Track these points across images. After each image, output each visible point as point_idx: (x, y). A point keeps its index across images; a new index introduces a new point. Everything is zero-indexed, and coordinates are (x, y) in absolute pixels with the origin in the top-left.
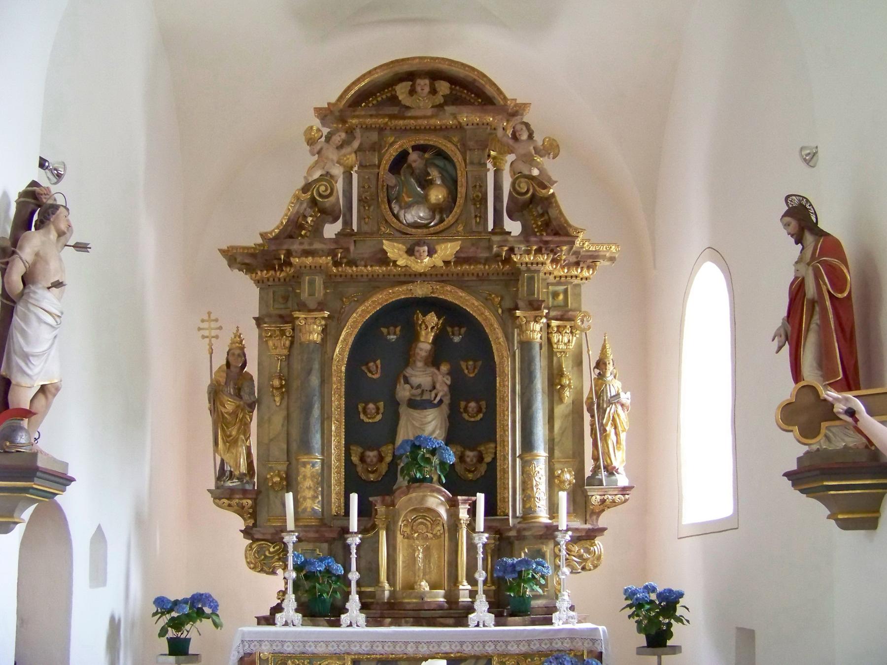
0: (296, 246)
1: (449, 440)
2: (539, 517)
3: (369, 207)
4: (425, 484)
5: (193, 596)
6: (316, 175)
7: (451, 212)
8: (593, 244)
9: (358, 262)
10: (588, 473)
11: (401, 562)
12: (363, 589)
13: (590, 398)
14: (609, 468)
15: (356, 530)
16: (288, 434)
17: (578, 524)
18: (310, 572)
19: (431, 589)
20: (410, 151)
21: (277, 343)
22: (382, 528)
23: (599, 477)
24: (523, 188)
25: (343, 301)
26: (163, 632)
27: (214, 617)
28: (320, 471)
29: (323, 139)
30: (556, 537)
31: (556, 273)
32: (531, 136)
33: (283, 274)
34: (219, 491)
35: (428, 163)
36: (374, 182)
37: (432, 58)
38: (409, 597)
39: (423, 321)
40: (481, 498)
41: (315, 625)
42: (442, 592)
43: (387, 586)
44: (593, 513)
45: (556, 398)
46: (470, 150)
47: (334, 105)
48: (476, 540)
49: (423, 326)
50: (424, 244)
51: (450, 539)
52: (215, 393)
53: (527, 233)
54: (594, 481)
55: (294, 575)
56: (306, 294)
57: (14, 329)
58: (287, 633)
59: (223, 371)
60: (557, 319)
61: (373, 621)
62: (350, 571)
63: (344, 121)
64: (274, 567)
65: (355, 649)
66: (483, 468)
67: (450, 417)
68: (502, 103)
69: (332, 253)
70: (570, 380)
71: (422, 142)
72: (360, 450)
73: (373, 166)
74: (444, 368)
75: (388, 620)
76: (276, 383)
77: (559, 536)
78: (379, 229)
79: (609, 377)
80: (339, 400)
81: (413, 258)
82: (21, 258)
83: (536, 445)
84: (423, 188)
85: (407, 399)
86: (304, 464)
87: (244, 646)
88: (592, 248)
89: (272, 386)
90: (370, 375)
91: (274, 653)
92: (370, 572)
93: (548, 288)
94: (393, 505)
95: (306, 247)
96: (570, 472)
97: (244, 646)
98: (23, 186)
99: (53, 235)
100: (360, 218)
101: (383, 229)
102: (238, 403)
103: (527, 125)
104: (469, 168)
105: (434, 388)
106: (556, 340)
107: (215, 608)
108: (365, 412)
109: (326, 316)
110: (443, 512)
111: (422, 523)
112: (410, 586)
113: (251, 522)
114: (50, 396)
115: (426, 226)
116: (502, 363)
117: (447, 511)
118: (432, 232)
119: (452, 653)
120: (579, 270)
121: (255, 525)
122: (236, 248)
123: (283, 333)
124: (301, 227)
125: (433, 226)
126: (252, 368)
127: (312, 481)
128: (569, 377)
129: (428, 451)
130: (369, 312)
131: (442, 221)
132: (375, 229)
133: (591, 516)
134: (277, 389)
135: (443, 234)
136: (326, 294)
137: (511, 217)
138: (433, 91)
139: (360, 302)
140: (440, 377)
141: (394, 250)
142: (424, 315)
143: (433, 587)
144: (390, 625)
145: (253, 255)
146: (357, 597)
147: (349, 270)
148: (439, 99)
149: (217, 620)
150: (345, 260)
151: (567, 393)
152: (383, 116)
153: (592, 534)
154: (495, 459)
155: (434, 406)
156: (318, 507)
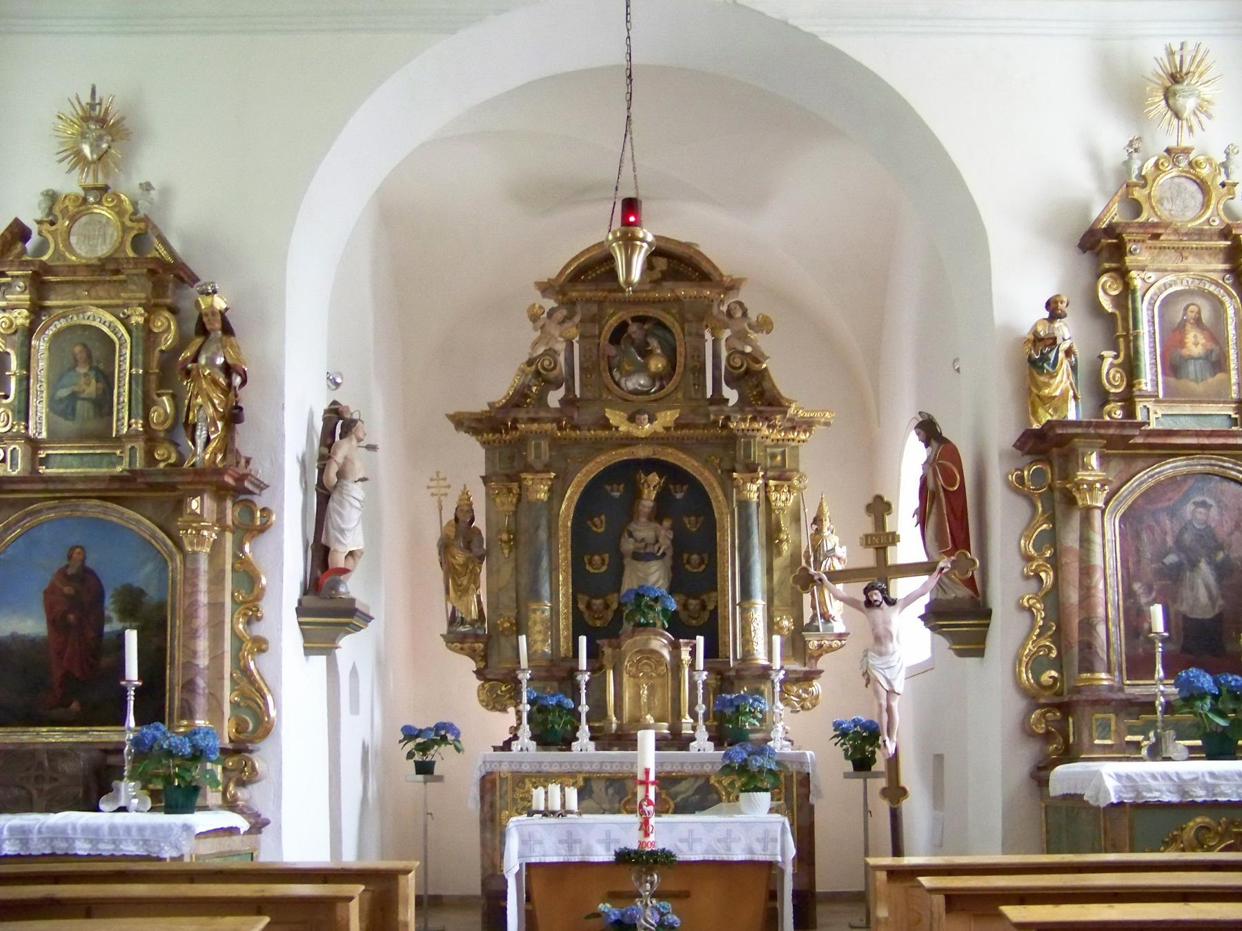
0: (522, 414)
1: (672, 591)
2: (757, 659)
3: (591, 375)
4: (649, 628)
6: (541, 350)
7: (670, 380)
8: (807, 411)
9: (582, 427)
10: (807, 620)
11: (627, 699)
12: (591, 724)
13: (807, 552)
14: (826, 616)
15: (585, 668)
16: (517, 584)
17: (796, 666)
18: (542, 705)
19: (655, 721)
20: (630, 322)
21: (504, 499)
22: (609, 668)
23: (816, 624)
24: (738, 362)
26: (410, 755)
27: (457, 743)
28: (549, 617)
29: (545, 315)
30: (770, 675)
31: (772, 437)
32: (745, 314)
34: (451, 635)
36: (595, 351)
39: (646, 481)
40: (700, 640)
42: (666, 724)
43: (614, 719)
44: (811, 657)
45: (775, 551)
46: (688, 322)
47: (553, 280)
48: (696, 677)
49: (646, 485)
50: (645, 412)
51: (673, 678)
52: (445, 547)
53: (743, 401)
54: (812, 627)
55: (528, 707)
56: (533, 456)
57: (332, 512)
59: (452, 526)
60: (774, 479)
62: (579, 704)
63: (564, 294)
64: (506, 705)
65: (587, 768)
66: (706, 616)
69: (558, 421)
70: (787, 535)
71: (641, 314)
72: (586, 598)
73: (594, 336)
74: (667, 523)
76: (505, 537)
77: (773, 674)
79: (826, 533)
80: (566, 552)
81: (634, 425)
82: (335, 461)
83: (753, 594)
84: (643, 356)
85: (631, 551)
86: (534, 611)
87: (486, 766)
88: (808, 415)
89: (501, 540)
90: (595, 529)
91: (513, 772)
92: (598, 710)
93: (766, 451)
94: (619, 646)
95: (532, 415)
96: (788, 620)
98: (325, 406)
99: (354, 442)
100: (582, 385)
102: (468, 555)
103: (740, 304)
104: (687, 338)
105: (657, 541)
106: (774, 499)
107: (457, 734)
108: (590, 563)
109: (552, 477)
110: (666, 653)
111: (646, 664)
113: (482, 665)
114: (357, 559)
115: (647, 393)
116: (722, 519)
117: (670, 653)
118: (652, 399)
119: (673, 772)
120: (796, 434)
121: (486, 667)
122: (463, 413)
124: (526, 396)
126: (480, 523)
127: (542, 625)
128: (787, 532)
129: (652, 599)
130: (593, 473)
131: (662, 388)
132: (597, 396)
133: (810, 659)
134: (505, 542)
135: (663, 402)
136: (551, 457)
137: (727, 384)
139: (585, 462)
140: (663, 532)
141: (616, 417)
142: (647, 474)
145: (479, 420)
147: (573, 434)
150: (569, 426)
151: (785, 547)
152: (603, 290)
153: (811, 676)
154: (716, 608)
155: (657, 558)
156: (547, 650)
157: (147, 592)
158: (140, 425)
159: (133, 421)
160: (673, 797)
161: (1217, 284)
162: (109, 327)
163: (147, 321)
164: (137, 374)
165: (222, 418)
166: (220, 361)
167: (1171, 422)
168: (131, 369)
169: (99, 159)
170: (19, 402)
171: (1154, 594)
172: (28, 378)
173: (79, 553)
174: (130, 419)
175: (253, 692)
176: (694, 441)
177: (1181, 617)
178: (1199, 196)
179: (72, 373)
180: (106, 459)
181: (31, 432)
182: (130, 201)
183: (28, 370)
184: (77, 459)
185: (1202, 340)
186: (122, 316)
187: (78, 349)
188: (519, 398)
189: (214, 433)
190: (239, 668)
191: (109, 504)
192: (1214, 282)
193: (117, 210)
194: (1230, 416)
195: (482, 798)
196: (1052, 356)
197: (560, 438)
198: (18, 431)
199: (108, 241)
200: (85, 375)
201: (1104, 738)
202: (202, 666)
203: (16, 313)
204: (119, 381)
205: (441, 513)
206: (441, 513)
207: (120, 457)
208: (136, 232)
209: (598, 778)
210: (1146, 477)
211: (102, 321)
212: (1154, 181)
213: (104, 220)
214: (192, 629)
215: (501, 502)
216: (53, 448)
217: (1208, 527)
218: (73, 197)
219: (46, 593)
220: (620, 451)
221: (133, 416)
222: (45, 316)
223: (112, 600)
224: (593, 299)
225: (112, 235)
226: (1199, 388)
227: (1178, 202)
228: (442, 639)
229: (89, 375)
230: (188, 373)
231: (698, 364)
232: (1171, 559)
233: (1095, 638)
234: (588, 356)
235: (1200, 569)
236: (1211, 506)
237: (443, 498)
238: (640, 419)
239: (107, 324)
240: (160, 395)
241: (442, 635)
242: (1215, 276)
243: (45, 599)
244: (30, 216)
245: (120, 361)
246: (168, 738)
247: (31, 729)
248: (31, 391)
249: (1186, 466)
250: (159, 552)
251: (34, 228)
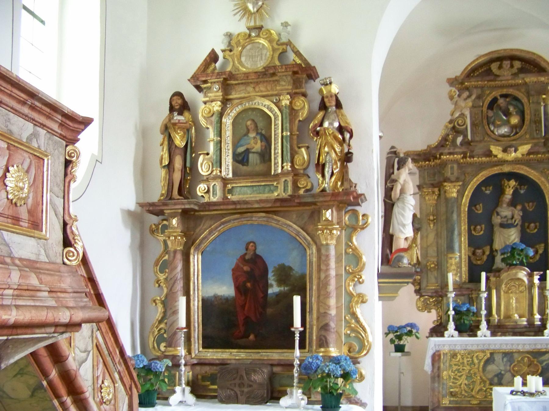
6: (457, 115)
20: (499, 98)
22: (494, 289)
25: (465, 176)
33: (433, 163)
35: (509, 103)
38: (509, 322)
39: (508, 184)
43: (496, 316)
49: (508, 187)
56: (449, 174)
58: (452, 341)
61: (493, 334)
65: (492, 347)
73: (479, 106)
74: (519, 207)
75: (499, 334)
86: (451, 258)
87: (436, 347)
89: (429, 219)
94: (499, 277)
95: (451, 151)
97: (436, 347)
110: (525, 279)
115: (509, 136)
117: (528, 279)
122: (410, 152)
123: (433, 192)
131: (516, 133)
132: (482, 139)
134: (432, 221)
138: (512, 66)
140: (516, 212)
141: (496, 150)
143: (520, 317)
144: (501, 336)
146: (485, 323)
148: (515, 70)
157: (293, 268)
158: (289, 167)
159: (285, 164)
160: (541, 363)
162: (268, 108)
163: (291, 103)
164: (287, 136)
165: (339, 160)
166: (336, 125)
168: (282, 132)
169: (257, 11)
170: (217, 156)
172: (220, 142)
173: (252, 246)
174: (282, 163)
175: (357, 327)
176: (536, 162)
179: (245, 137)
180: (267, 189)
181: (223, 174)
182: (276, 33)
183: (221, 137)
184: (250, 189)
186: (275, 101)
187: (249, 123)
188: (443, 143)
189: (335, 169)
190: (350, 313)
191: (270, 215)
193: (268, 39)
195: (433, 365)
197: (462, 163)
198: (216, 174)
199: (264, 58)
200: (254, 138)
202: (333, 315)
203: (213, 104)
204: (275, 140)
207: (276, 186)
208: (281, 51)
209: (499, 352)
211: (263, 105)
213: (261, 46)
214: (327, 292)
215: (429, 199)
216: (236, 183)
218: (243, 34)
219: (233, 270)
220: (493, 169)
221: (284, 161)
222: (229, 104)
223: (272, 274)
224: (479, 86)
225: (266, 55)
229: (257, 138)
230: (317, 134)
231: (539, 119)
234: (477, 117)
238: (510, 150)
239: (266, 106)
240: (299, 148)
243: (233, 274)
244: (219, 47)
245: (275, 128)
246: (327, 366)
247: (227, 350)
248: (222, 150)
250: (301, 244)
251: (221, 55)
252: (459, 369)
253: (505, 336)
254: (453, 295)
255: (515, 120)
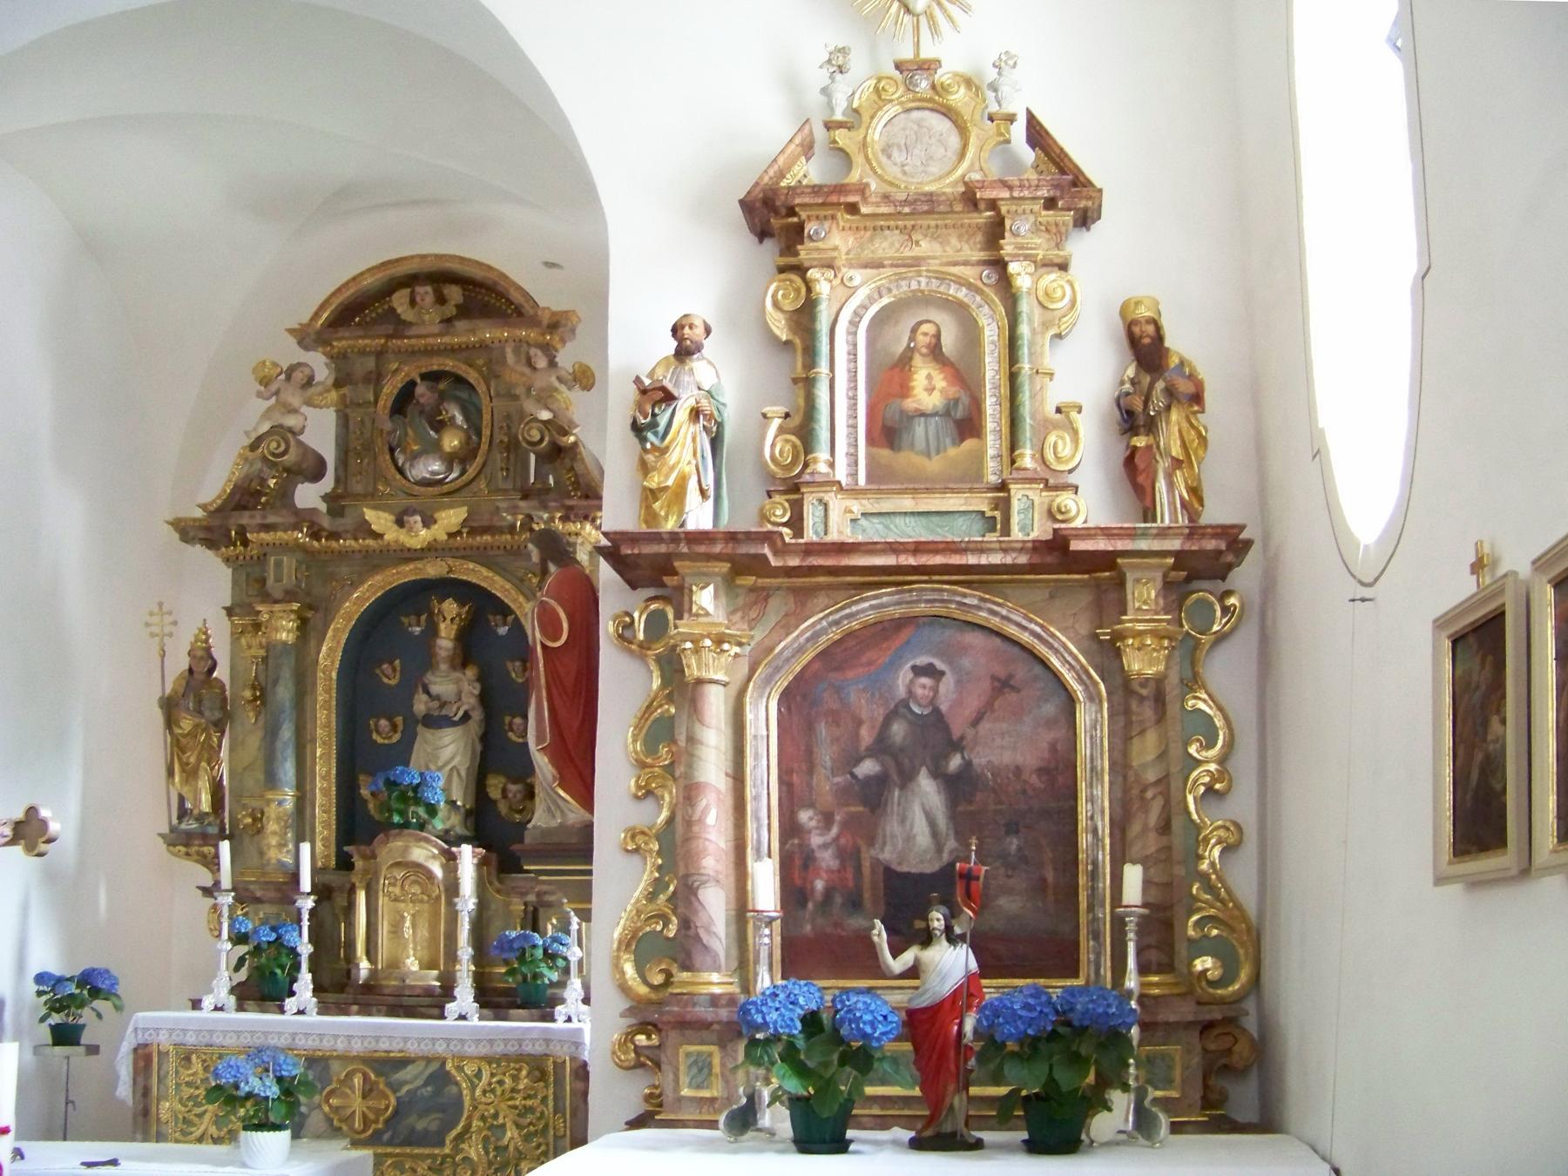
4: (406, 831)
5: (83, 974)
6: (265, 427)
19: (421, 968)
20: (419, 381)
29: (283, 377)
37: (436, 256)
41: (264, 1011)
42: (435, 973)
50: (414, 512)
52: (170, 707)
67: (485, 738)
68: (531, 312)
71: (435, 368)
73: (367, 403)
78: (376, 489)
94: (374, 856)
101: (381, 488)
108: (378, 733)
110: (438, 871)
112: (395, 964)
117: (443, 866)
125: (451, 481)
126: (222, 673)
127: (278, 823)
132: (370, 489)
138: (441, 300)
139: (354, 586)
141: (379, 520)
142: (441, 601)
144: (359, 1013)
147: (334, 544)
148: (450, 310)
149: (117, 1002)
152: (379, 337)
155: (455, 724)
161: (970, 286)
167: (880, 527)
171: (835, 830)
177: (881, 869)
178: (954, 141)
185: (940, 382)
192: (961, 282)
194: (983, 513)
196: (663, 421)
201: (699, 1087)
205: (163, 662)
206: (163, 662)
210: (824, 623)
212: (872, 118)
217: (936, 711)
226: (934, 465)
227: (916, 151)
228: (160, 840)
232: (868, 768)
233: (696, 912)
235: (919, 786)
236: (942, 673)
237: (166, 639)
241: (160, 835)
242: (969, 273)
249: (898, 603)
252: (198, 1096)
253: (370, 1014)
254: (230, 900)
255: (451, 442)
